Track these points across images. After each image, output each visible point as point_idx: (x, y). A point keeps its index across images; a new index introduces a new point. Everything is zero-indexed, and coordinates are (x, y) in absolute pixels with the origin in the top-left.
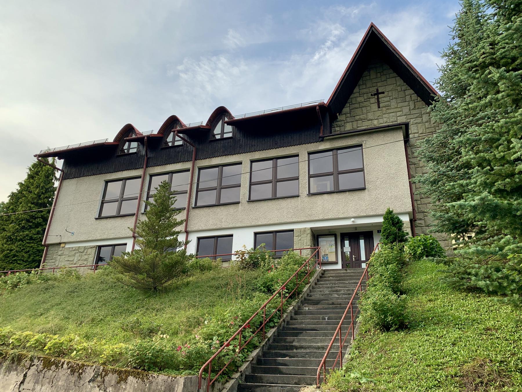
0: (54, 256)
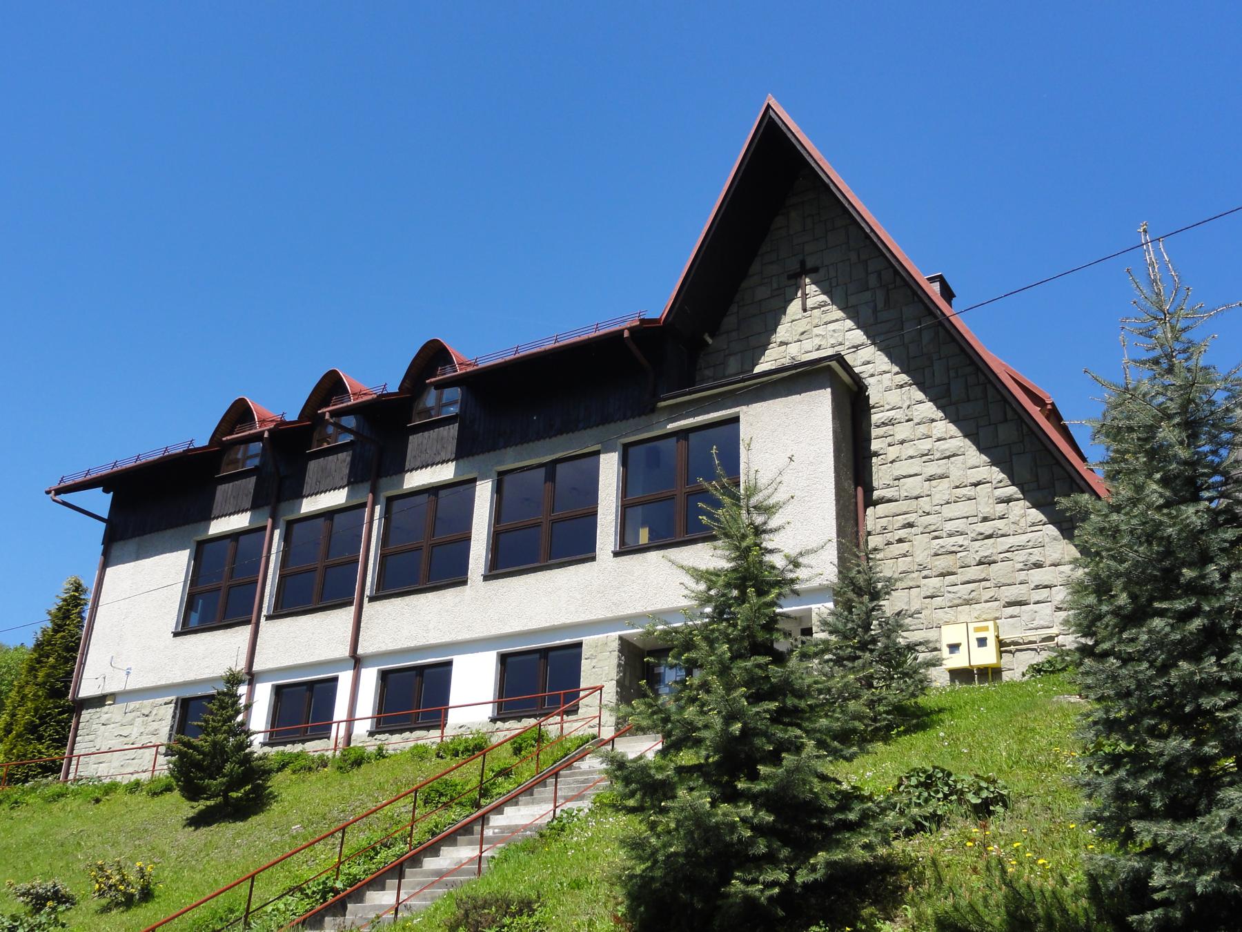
0: (94, 726)
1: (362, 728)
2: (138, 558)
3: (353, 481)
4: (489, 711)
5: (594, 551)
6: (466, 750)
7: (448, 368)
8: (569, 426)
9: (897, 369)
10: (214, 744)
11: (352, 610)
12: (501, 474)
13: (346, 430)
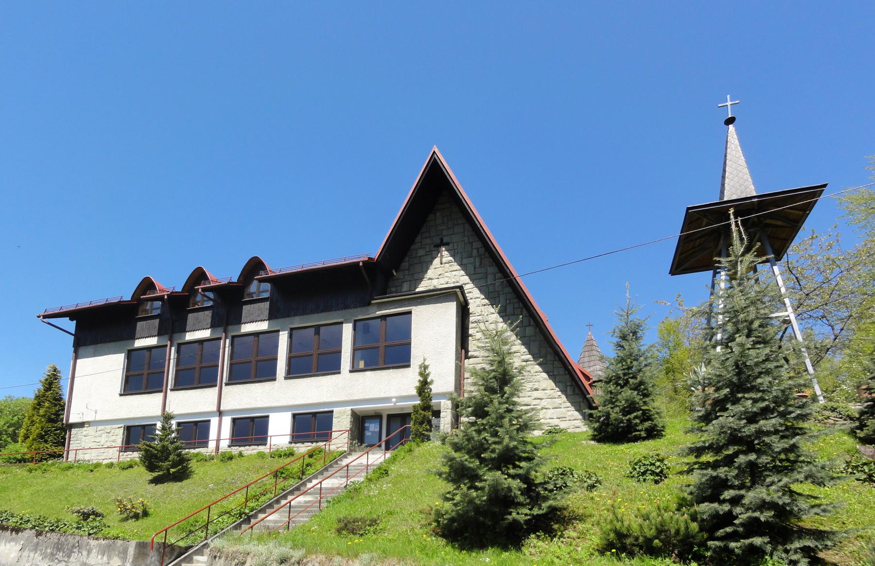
1: (224, 444)
2: (94, 356)
3: (213, 326)
4: (288, 439)
5: (409, 361)
6: (285, 455)
7: (262, 272)
8: (327, 309)
9: (483, 297)
10: (163, 446)
11: (217, 389)
12: (292, 329)
13: (210, 299)
